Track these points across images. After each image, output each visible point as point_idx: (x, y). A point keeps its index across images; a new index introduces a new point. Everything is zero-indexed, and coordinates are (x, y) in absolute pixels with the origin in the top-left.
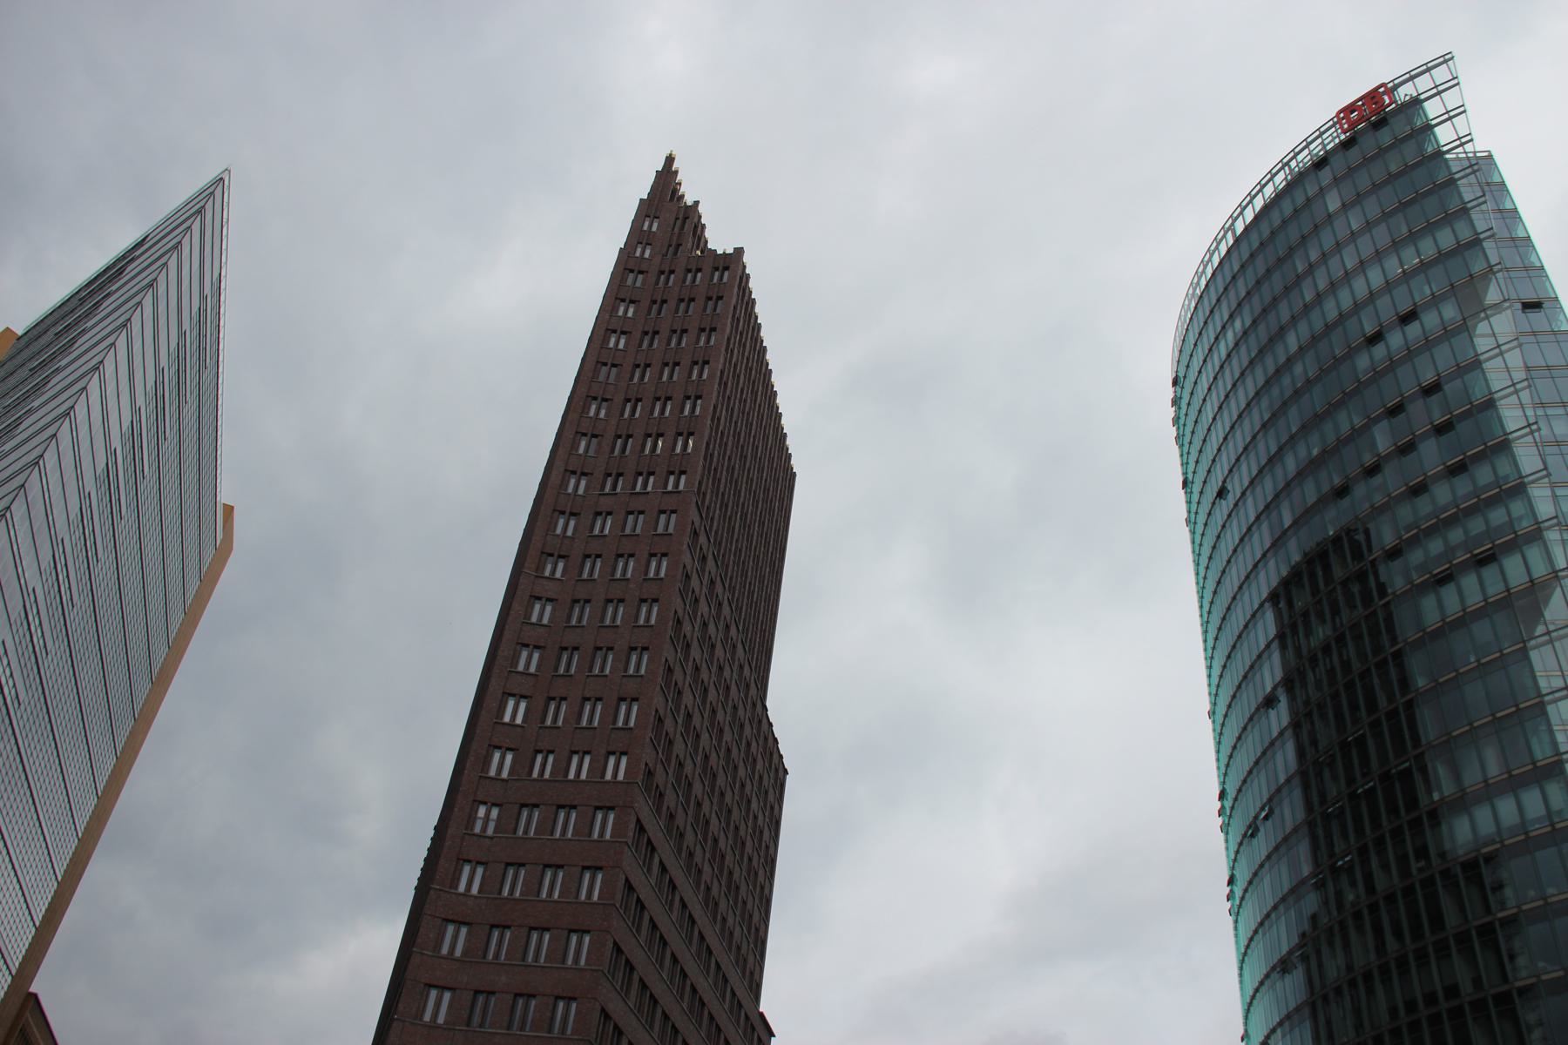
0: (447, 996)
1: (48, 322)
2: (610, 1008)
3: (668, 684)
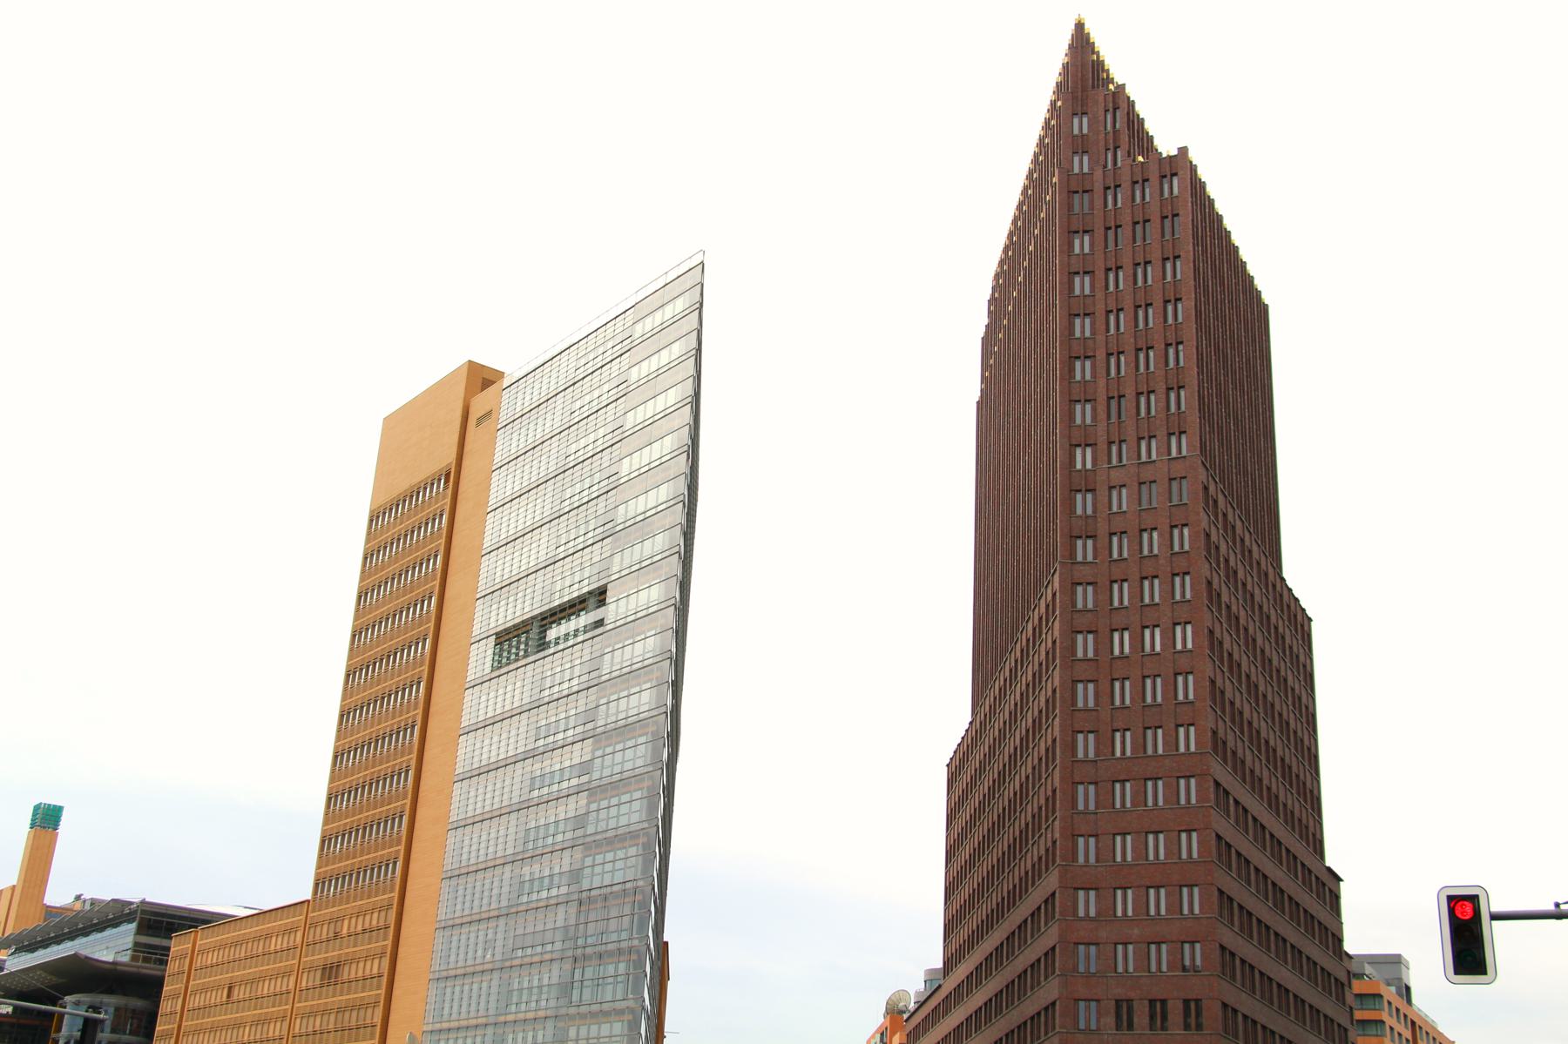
2: (1231, 1001)
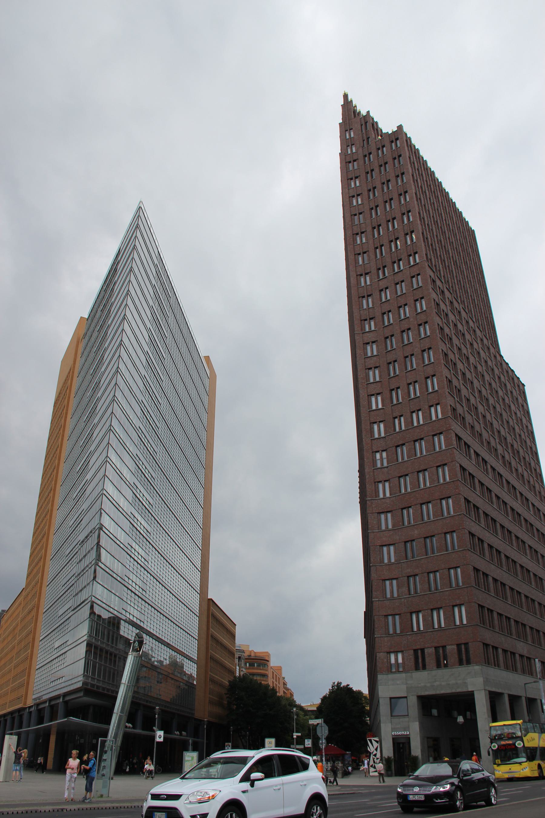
0: (392, 548)
1: (96, 307)
2: (473, 531)
3: (447, 362)
